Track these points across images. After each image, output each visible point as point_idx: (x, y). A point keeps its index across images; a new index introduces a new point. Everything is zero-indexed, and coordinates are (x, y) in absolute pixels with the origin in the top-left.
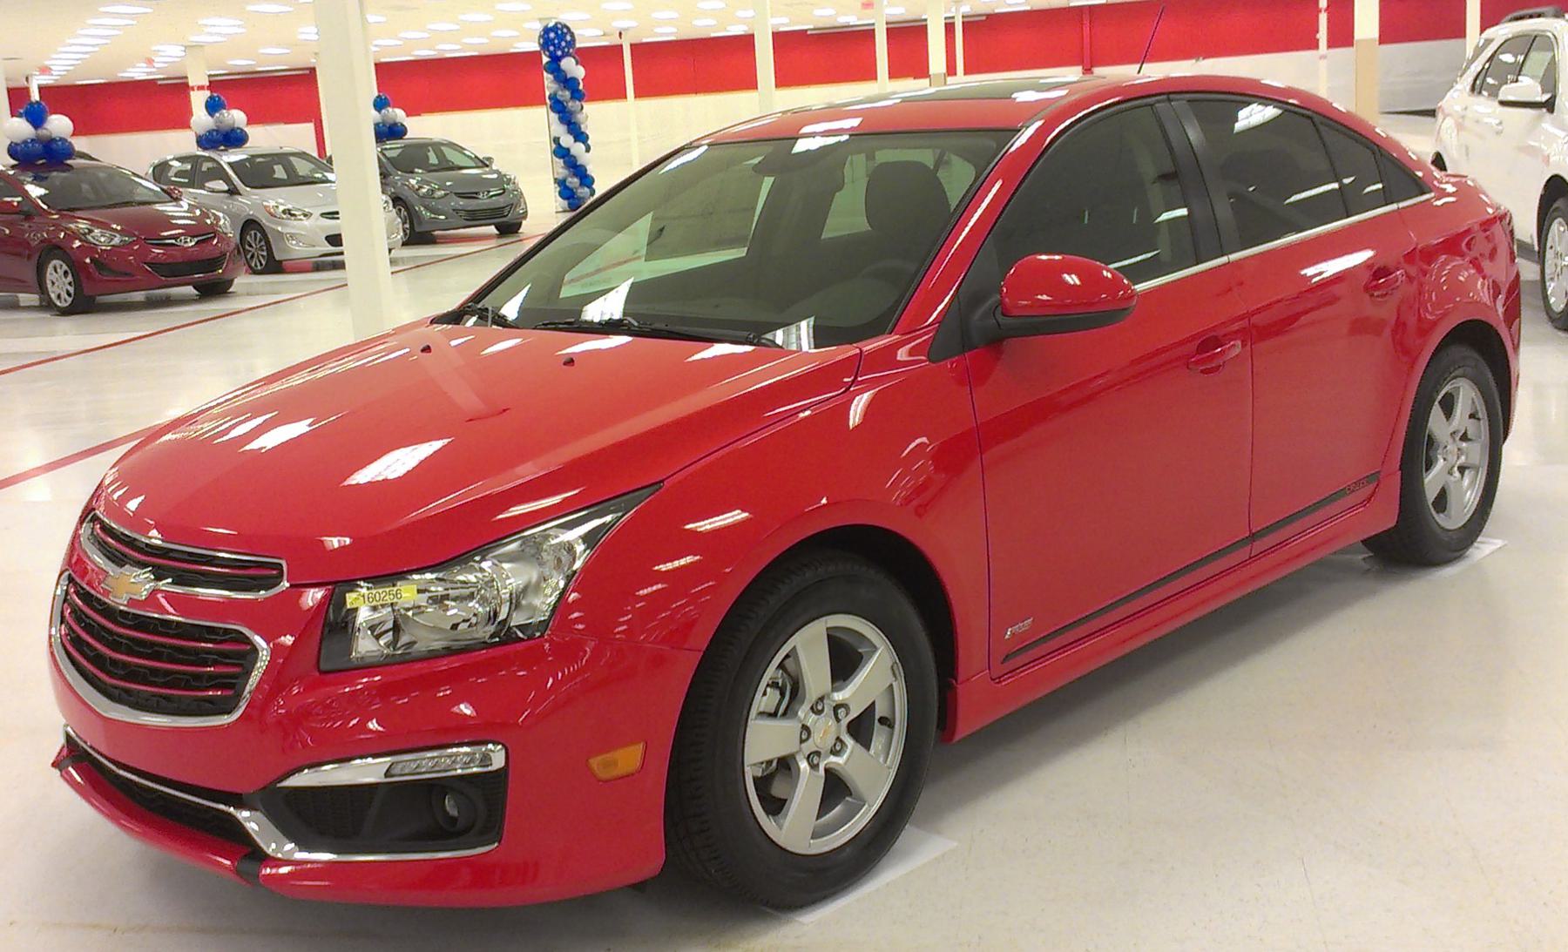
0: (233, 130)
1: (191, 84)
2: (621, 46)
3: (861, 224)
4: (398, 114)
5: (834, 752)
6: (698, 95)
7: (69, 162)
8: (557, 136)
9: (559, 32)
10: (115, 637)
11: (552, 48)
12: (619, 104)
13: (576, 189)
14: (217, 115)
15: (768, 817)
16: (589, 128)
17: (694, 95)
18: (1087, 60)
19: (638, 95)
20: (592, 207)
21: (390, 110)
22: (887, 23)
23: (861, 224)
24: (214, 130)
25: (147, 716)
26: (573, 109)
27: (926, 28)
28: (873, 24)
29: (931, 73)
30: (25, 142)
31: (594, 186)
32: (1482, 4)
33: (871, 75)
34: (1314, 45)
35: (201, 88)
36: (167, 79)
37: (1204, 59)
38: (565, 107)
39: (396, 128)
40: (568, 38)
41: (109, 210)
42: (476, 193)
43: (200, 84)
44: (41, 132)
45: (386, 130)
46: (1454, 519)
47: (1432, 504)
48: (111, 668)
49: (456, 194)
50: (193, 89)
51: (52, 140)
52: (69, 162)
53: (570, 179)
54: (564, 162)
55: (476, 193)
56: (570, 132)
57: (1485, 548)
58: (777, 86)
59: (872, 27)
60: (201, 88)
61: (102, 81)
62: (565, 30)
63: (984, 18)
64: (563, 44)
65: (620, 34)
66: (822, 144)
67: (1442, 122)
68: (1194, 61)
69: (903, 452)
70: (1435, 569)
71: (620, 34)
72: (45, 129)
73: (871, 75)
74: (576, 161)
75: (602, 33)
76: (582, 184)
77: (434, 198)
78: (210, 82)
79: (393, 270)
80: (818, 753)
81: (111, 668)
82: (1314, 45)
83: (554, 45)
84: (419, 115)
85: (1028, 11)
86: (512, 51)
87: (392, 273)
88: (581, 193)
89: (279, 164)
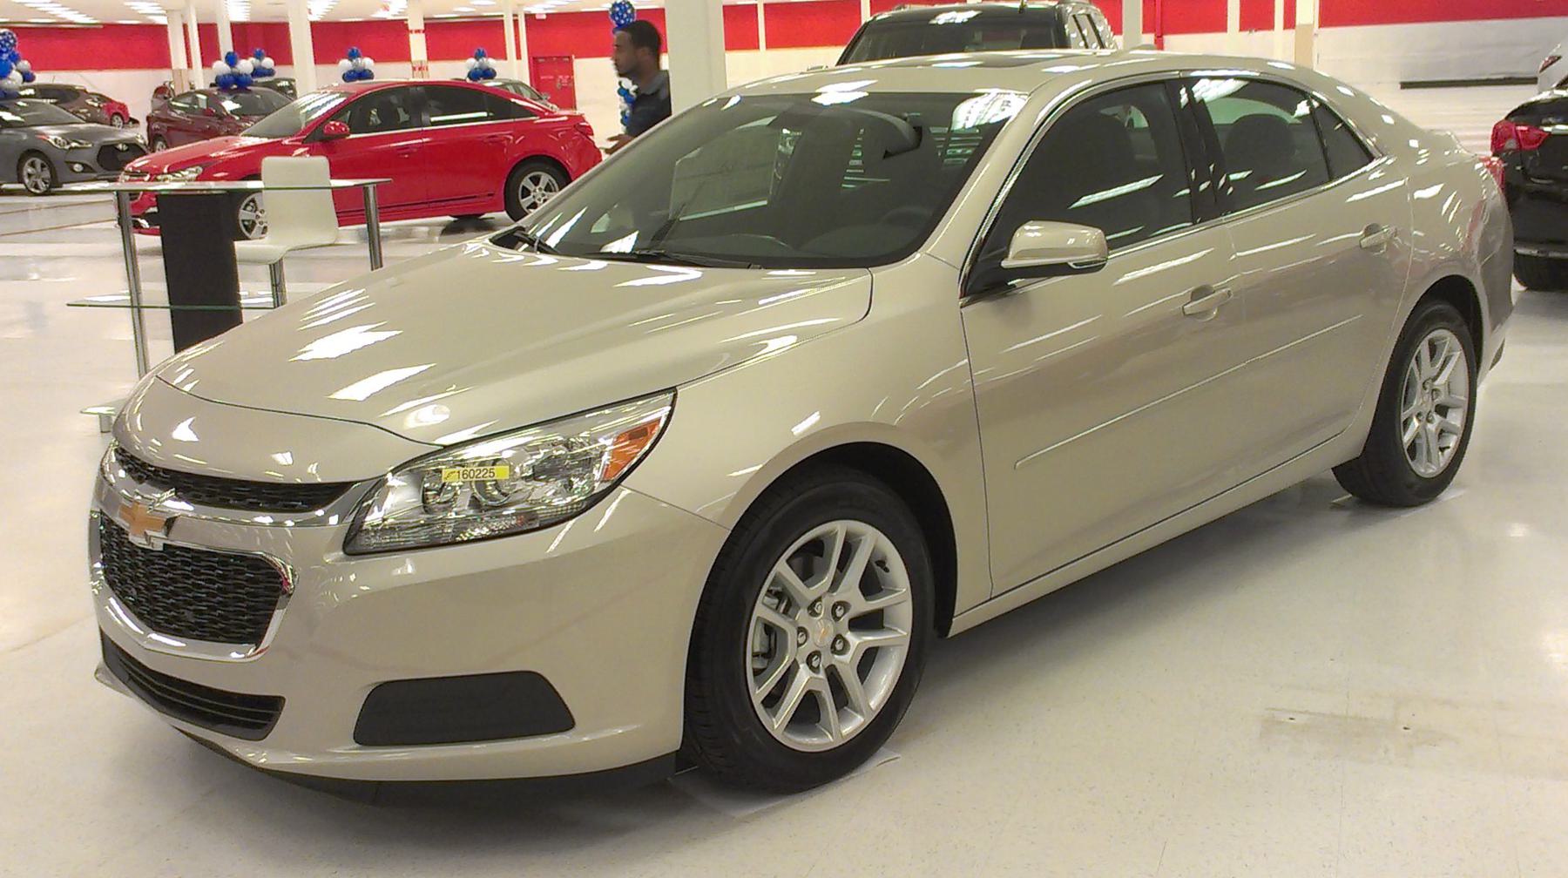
1: (410, 28)
2: (756, 5)
4: (367, 62)
5: (834, 650)
7: (249, 88)
9: (623, 8)
11: (617, 18)
14: (354, 61)
18: (1158, 28)
19: (769, 46)
21: (485, 59)
22: (424, 19)
25: (303, 765)
28: (502, 16)
29: (1297, 23)
30: (224, 76)
32: (1322, 7)
33: (1221, 26)
34: (756, 47)
35: (418, 31)
36: (461, 17)
37: (1256, 31)
40: (629, 11)
43: (418, 28)
44: (234, 70)
45: (481, 72)
46: (1428, 468)
47: (1408, 450)
48: (139, 198)
50: (411, 32)
51: (240, 75)
52: (249, 88)
57: (1449, 495)
58: (726, 49)
59: (500, 18)
60: (418, 31)
61: (360, 20)
62: (627, 6)
64: (625, 16)
66: (1277, 114)
68: (1248, 32)
70: (1403, 511)
72: (9, 79)
73: (1221, 26)
78: (425, 25)
79: (1425, 458)
80: (817, 653)
81: (139, 198)
82: (757, 47)
83: (618, 16)
85: (656, 9)
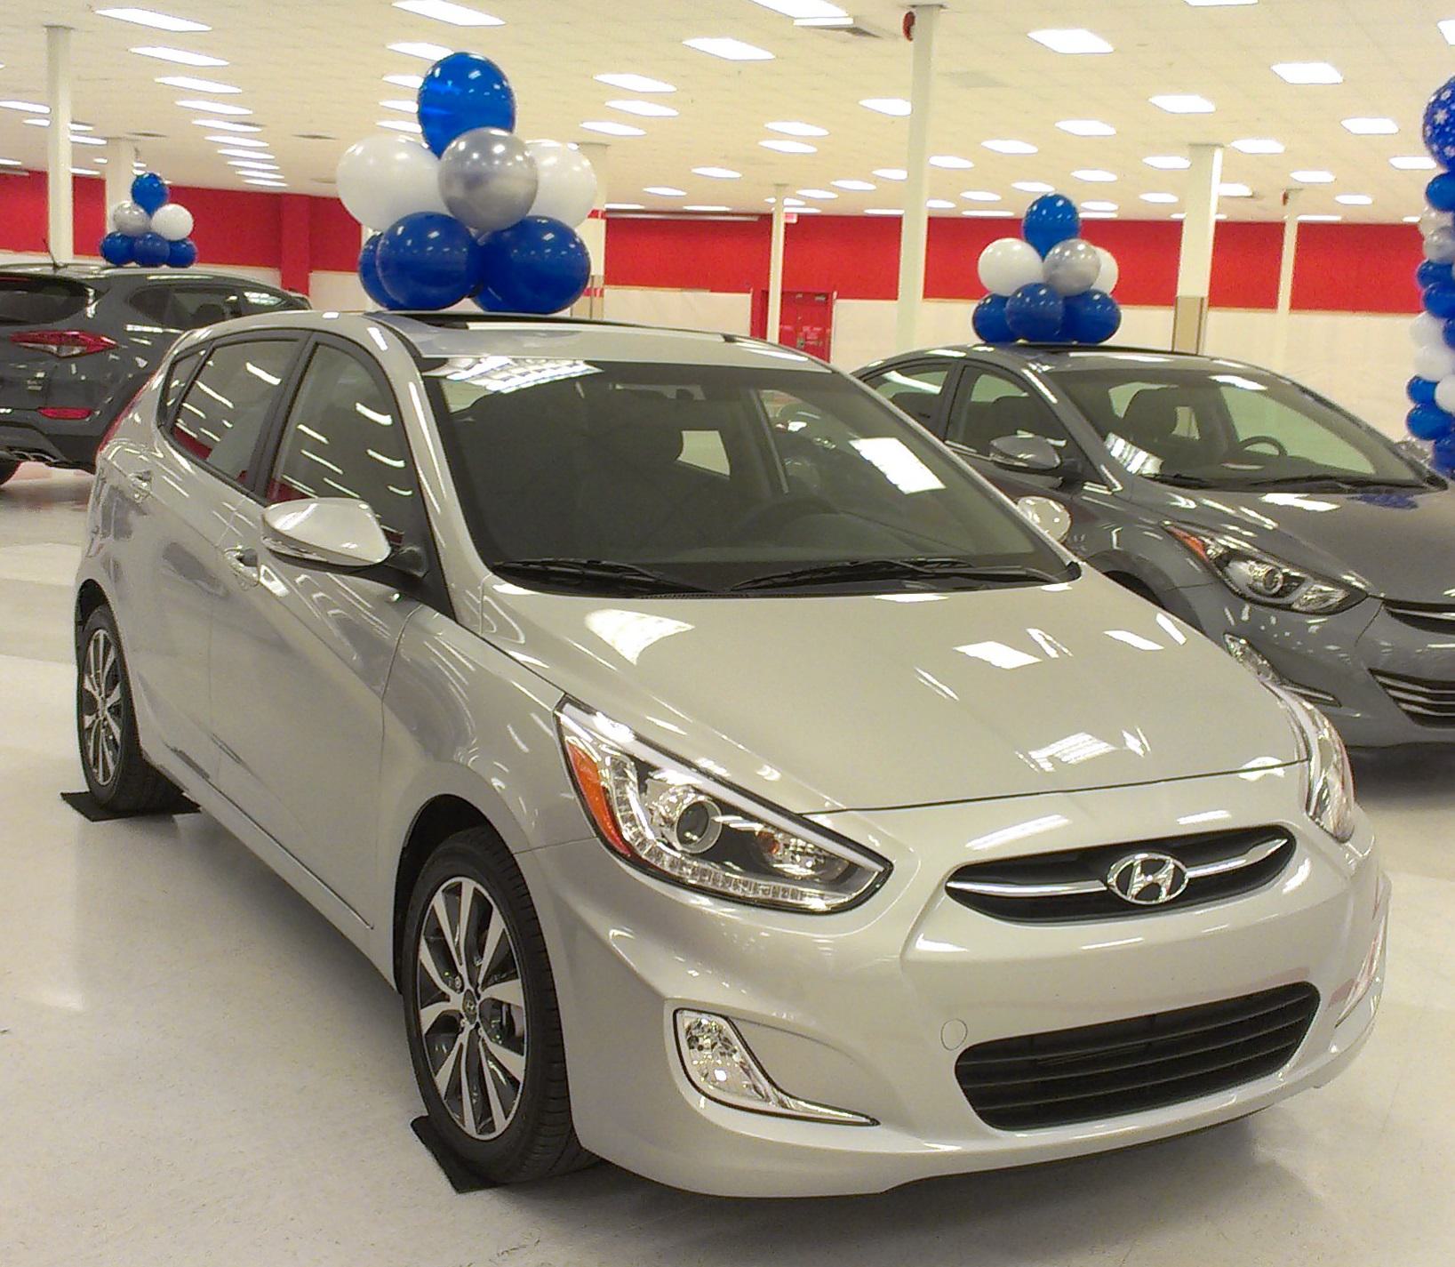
0: (527, 229)
3: (389, 417)
6: (1357, 313)
8: (1428, 376)
15: (122, 267)
17: (1352, 312)
19: (1298, 303)
20: (749, 795)
23: (389, 417)
24: (430, 220)
27: (900, 224)
34: (1269, 302)
41: (421, 908)
63: (755, 219)
65: (1285, 197)
67: (1123, 451)
71: (1285, 197)
75: (1250, 194)
82: (1269, 302)
87: (334, 182)
89: (940, 393)
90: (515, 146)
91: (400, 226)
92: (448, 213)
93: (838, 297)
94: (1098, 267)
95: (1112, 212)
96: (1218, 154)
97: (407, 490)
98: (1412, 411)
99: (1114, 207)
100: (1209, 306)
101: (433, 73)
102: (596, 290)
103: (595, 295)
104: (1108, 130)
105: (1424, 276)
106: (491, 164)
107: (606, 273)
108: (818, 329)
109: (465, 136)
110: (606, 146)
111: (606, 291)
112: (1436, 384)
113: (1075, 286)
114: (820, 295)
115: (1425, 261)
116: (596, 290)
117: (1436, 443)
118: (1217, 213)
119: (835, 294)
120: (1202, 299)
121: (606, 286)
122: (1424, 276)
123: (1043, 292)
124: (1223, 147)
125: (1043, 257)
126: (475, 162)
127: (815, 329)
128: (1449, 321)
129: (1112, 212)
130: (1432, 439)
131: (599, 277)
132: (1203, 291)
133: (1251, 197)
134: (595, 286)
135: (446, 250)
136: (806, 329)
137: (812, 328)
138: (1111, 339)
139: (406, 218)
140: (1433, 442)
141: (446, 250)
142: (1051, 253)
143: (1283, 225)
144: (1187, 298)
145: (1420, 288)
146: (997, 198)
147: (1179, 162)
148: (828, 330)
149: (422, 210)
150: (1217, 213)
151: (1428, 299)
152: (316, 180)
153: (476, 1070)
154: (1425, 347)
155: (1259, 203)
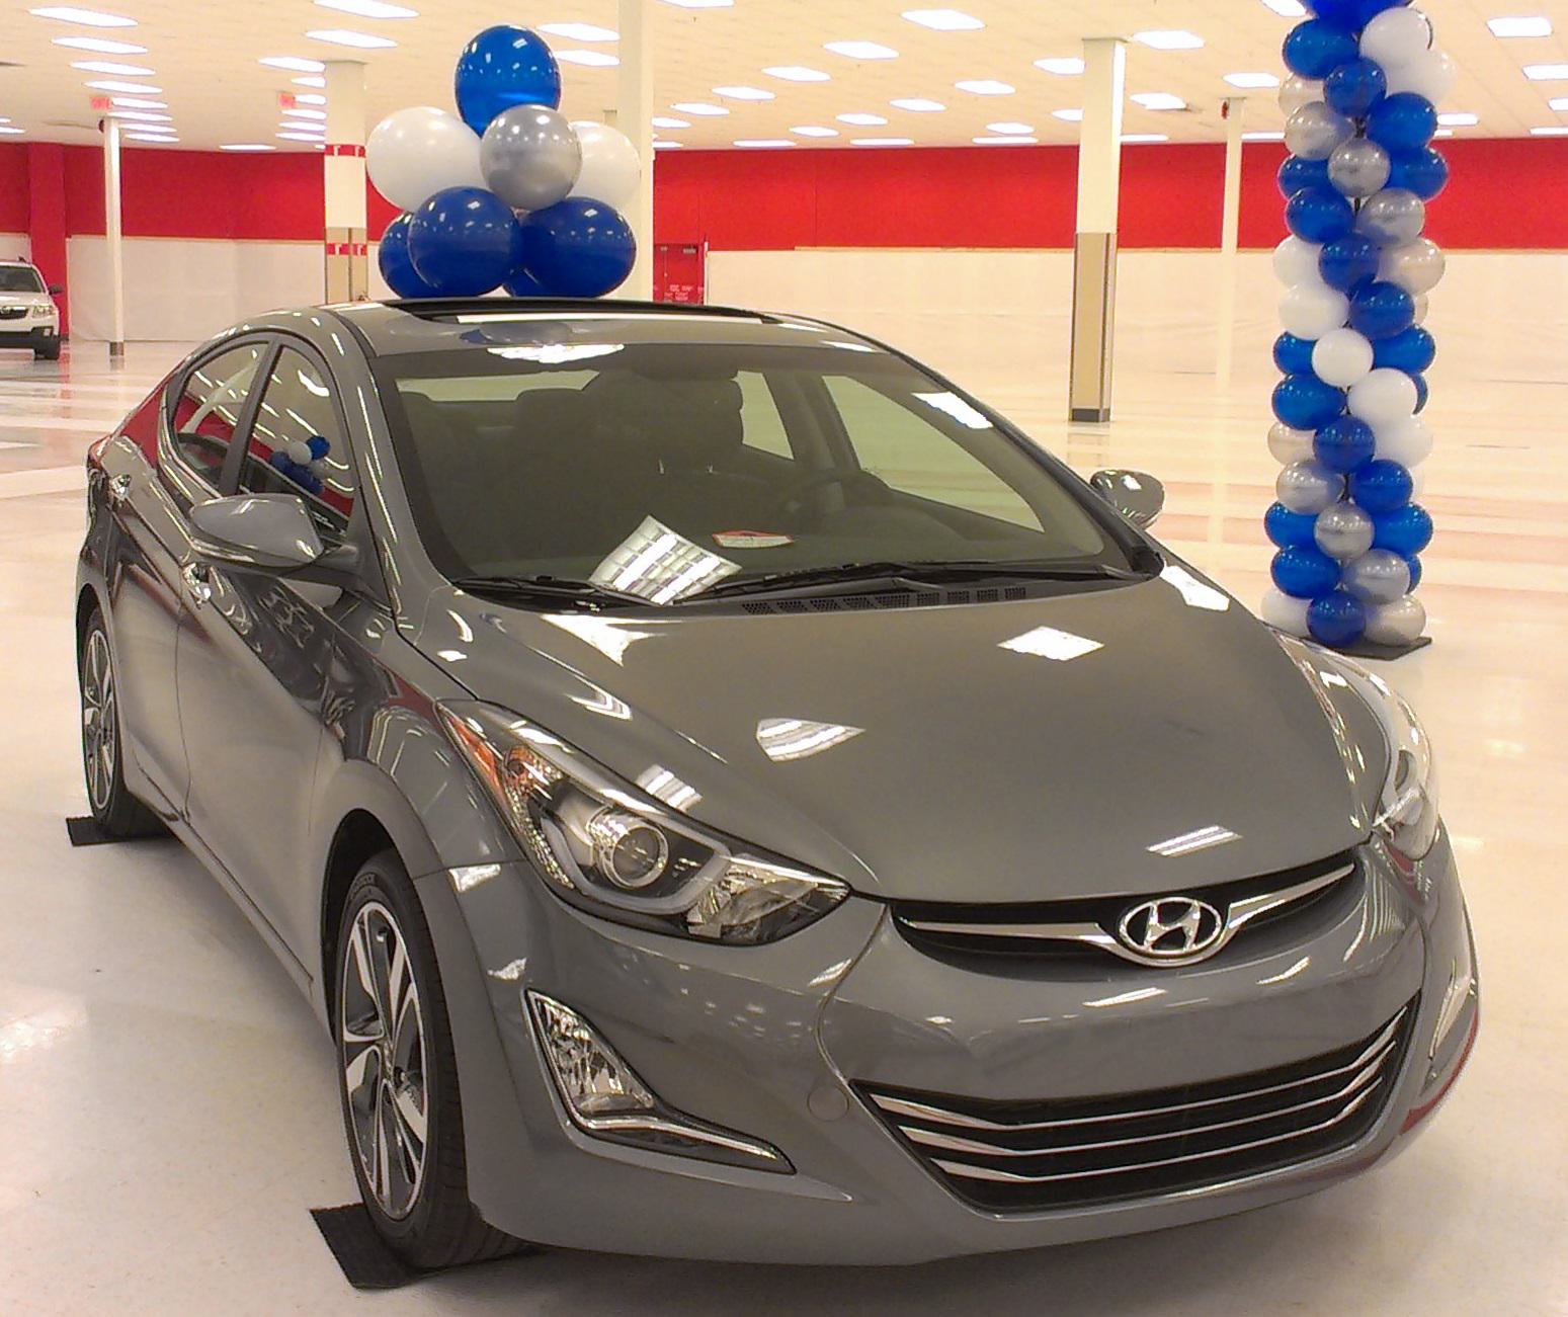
8: (1299, 333)
10: (521, 584)
12: (1053, 255)
13: (1358, 559)
16: (1432, 316)
26: (1390, 229)
31: (1422, 557)
38: (1352, 215)
39: (565, 236)
42: (1104, 912)
45: (500, 234)
49: (902, 909)
53: (1333, 520)
54: (1319, 444)
55: (1104, 912)
56: (1357, 321)
65: (1225, 108)
69: (1360, 766)
71: (1225, 108)
74: (1371, 444)
75: (1184, 106)
76: (1382, 545)
77: (677, 925)
82: (1213, 240)
84: (793, 249)
86: (981, 141)
88: (1374, 577)
90: (560, 125)
91: (595, 209)
92: (487, 189)
93: (709, 250)
94: (578, 157)
95: (1027, 135)
96: (1120, 49)
97: (344, 465)
98: (1281, 384)
99: (1029, 129)
100: (1119, 245)
101: (470, 50)
102: (356, 246)
103: (356, 253)
104: (970, 23)
105: (1290, 180)
106: (534, 138)
107: (368, 224)
108: (689, 288)
109: (504, 114)
110: (362, 64)
111: (369, 247)
112: (1312, 344)
113: (539, 190)
114: (689, 247)
115: (1292, 157)
116: (356, 246)
117: (1316, 434)
118: (1122, 134)
119: (706, 244)
120: (1108, 235)
121: (371, 242)
122: (1290, 180)
123: (474, 205)
124: (1126, 42)
125: (480, 133)
126: (515, 137)
127: (684, 288)
128: (1325, 247)
129: (1027, 135)
130: (1310, 429)
131: (361, 229)
132: (1111, 227)
133: (1185, 110)
134: (354, 242)
135: (489, 225)
136: (674, 288)
137: (680, 288)
138: (616, 291)
139: (438, 194)
140: (1314, 432)
141: (489, 225)
142: (493, 124)
143: (1224, 145)
144: (1086, 234)
145: (1285, 197)
146: (882, 121)
147: (1073, 65)
148: (700, 289)
149: (458, 185)
150: (1122, 134)
151: (1295, 214)
152: (49, 123)
153: (371, 1082)
154: (1295, 287)
155: (1198, 118)
